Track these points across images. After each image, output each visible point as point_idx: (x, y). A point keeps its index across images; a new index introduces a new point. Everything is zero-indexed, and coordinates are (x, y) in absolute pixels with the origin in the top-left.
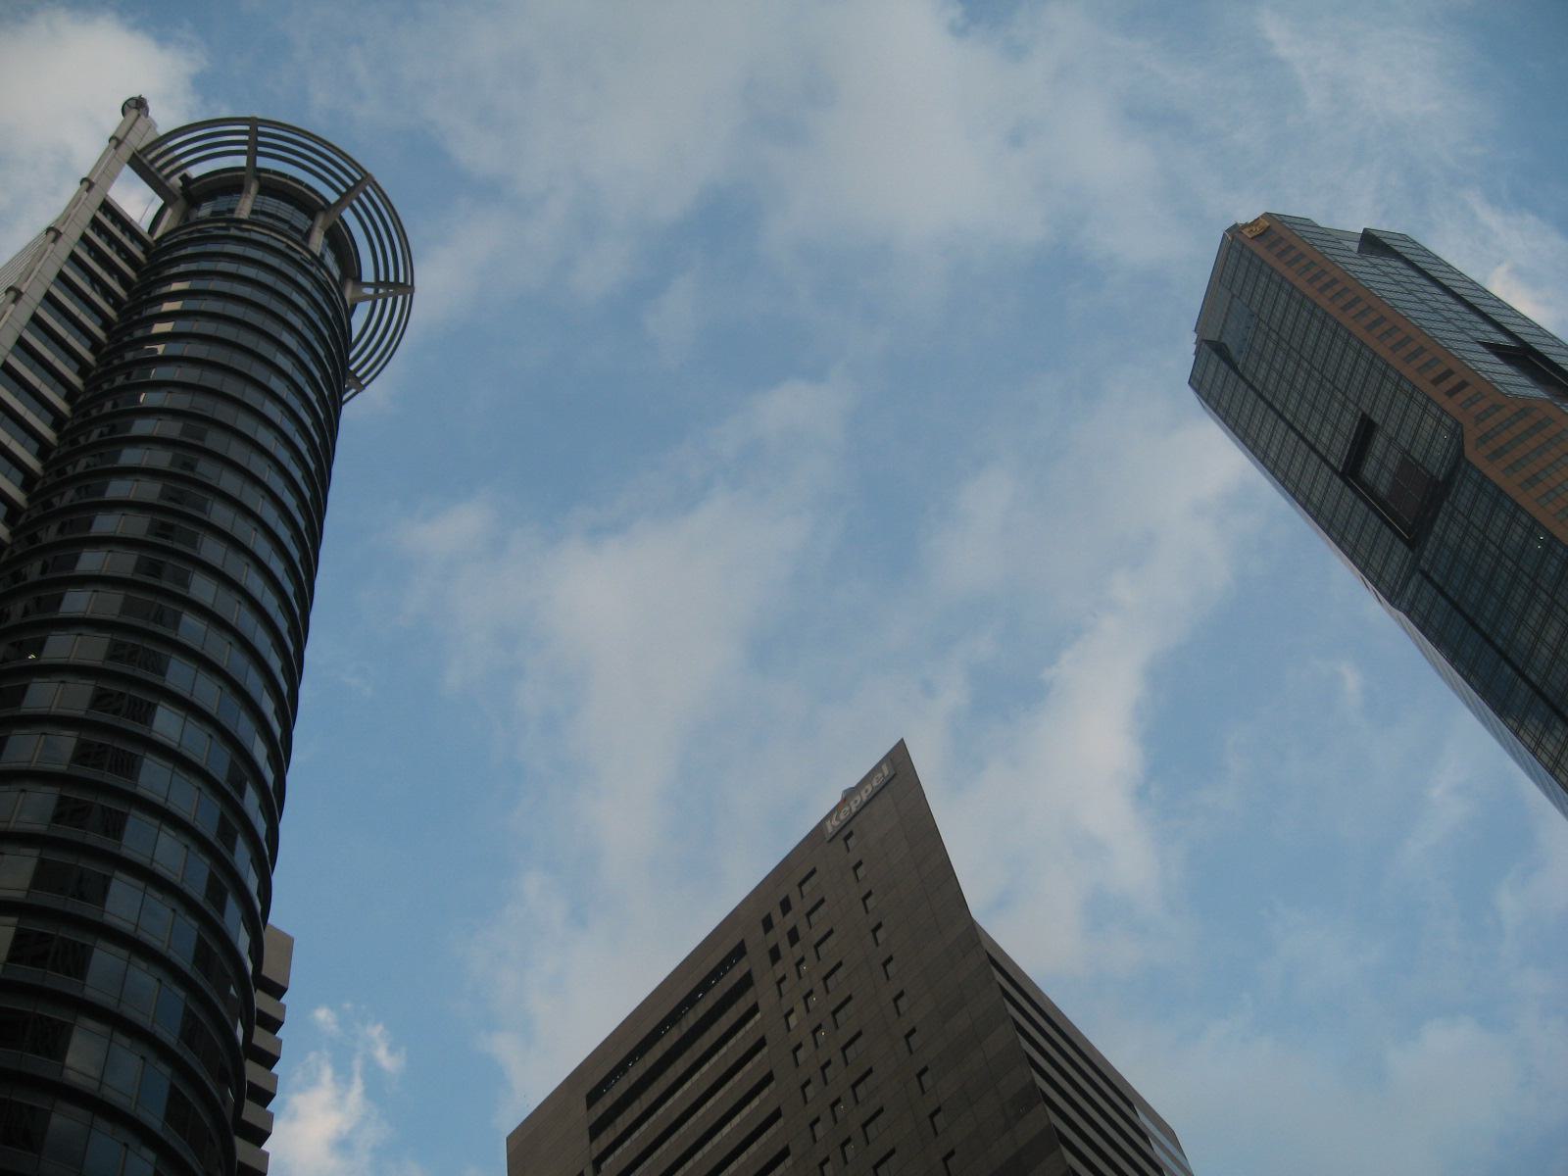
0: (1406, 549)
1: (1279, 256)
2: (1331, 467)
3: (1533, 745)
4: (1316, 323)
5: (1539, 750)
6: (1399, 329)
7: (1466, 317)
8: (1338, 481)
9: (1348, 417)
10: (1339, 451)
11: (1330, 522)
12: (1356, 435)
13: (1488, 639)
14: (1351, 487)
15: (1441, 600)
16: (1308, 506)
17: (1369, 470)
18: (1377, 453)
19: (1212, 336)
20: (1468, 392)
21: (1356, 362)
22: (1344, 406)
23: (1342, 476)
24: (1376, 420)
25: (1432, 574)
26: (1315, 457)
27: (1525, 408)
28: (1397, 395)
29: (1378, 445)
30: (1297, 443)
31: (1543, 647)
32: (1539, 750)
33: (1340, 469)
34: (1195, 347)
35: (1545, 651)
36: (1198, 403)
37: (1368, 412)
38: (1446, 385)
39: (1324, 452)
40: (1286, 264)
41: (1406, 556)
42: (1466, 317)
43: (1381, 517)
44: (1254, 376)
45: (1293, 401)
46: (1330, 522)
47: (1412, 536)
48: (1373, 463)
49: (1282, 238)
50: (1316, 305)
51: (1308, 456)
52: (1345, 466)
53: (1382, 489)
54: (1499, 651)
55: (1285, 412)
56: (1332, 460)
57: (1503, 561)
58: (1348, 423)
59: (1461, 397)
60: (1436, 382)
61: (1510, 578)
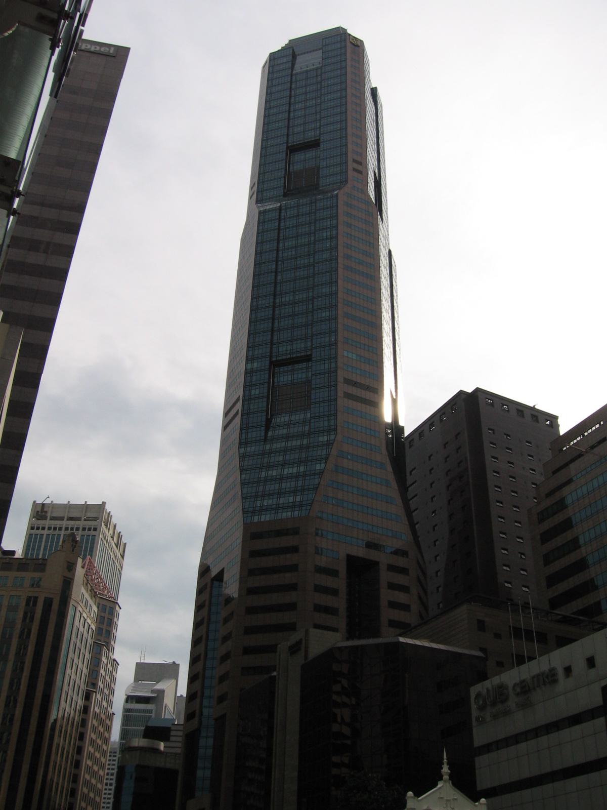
0: (282, 194)
2: (287, 141)
4: (339, 72)
8: (285, 147)
10: (296, 139)
11: (268, 124)
12: (308, 142)
13: (289, 112)
14: (287, 154)
16: (257, 266)
17: (299, 156)
18: (307, 156)
19: (297, 51)
21: (337, 114)
22: (315, 129)
23: (288, 147)
24: (322, 146)
25: (283, 211)
28: (338, 140)
29: (310, 154)
30: (288, 82)
31: (282, 456)
33: (290, 145)
34: (280, 48)
38: (356, 166)
39: (290, 133)
44: (295, 103)
45: (300, 106)
46: (268, 124)
47: (289, 193)
48: (302, 157)
50: (346, 89)
52: (292, 146)
55: (283, 221)
56: (290, 139)
58: (310, 136)
60: (354, 161)
61: (293, 414)
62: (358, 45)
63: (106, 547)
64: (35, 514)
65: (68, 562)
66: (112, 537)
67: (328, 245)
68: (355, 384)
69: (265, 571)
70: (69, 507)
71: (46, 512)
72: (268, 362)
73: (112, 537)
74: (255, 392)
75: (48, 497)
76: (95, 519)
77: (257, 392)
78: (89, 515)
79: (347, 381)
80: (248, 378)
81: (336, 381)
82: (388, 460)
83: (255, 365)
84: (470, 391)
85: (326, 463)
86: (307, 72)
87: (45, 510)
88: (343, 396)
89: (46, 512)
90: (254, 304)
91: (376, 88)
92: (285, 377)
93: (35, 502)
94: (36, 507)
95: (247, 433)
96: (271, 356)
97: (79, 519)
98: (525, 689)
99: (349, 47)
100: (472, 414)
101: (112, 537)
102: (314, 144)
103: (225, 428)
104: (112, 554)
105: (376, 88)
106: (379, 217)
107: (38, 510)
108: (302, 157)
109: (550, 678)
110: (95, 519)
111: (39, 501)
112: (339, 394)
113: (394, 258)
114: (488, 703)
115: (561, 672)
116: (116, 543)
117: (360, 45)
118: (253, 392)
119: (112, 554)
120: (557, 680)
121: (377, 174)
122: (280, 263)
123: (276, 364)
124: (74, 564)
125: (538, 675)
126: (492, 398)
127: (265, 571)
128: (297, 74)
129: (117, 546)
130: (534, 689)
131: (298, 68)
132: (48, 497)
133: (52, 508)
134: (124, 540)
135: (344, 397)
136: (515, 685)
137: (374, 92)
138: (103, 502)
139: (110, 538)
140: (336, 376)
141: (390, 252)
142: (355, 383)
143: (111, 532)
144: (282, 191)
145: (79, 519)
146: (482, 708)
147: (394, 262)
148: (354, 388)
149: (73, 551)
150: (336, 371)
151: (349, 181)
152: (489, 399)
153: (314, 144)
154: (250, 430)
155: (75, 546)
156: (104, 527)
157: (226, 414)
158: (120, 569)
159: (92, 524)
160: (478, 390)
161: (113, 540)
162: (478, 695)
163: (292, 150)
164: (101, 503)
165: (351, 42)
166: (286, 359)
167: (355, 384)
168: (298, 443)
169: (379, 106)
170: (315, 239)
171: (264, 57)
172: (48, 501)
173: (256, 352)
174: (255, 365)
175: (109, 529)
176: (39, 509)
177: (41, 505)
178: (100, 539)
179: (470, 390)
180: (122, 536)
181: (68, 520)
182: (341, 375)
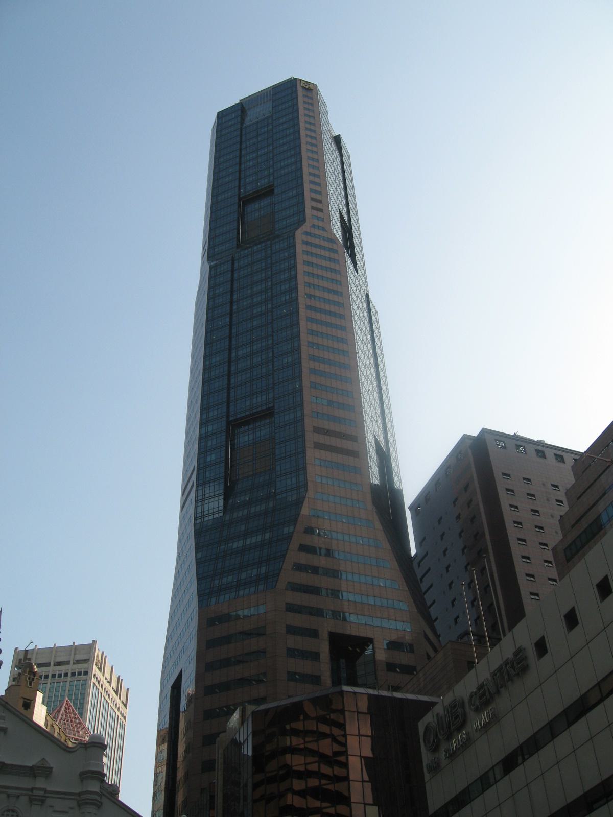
0: (236, 246)
1: (304, 96)
3: (200, 498)
5: (200, 504)
6: (319, 170)
7: (363, 301)
8: (237, 199)
9: (266, 180)
15: (237, 174)
17: (251, 207)
20: (320, 214)
24: (276, 191)
26: (229, 275)
27: (333, 240)
29: (264, 202)
32: (200, 504)
35: (249, 291)
36: (214, 121)
37: (275, 185)
40: (304, 107)
41: (218, 512)
42: (363, 301)
43: (227, 458)
49: (314, 117)
51: (226, 293)
53: (241, 440)
54: (229, 371)
57: (269, 338)
58: (263, 183)
59: (315, 213)
62: (310, 89)
63: (101, 694)
64: (18, 662)
65: (24, 698)
66: (108, 682)
67: (287, 287)
68: (327, 433)
69: (226, 663)
70: (56, 651)
71: (30, 659)
72: (224, 423)
73: (110, 682)
74: (212, 458)
75: (32, 642)
76: (86, 661)
77: (213, 457)
78: (78, 657)
79: (317, 430)
80: (203, 444)
81: (303, 430)
82: (376, 517)
83: (210, 428)
84: (476, 435)
85: (295, 525)
86: (257, 122)
87: (29, 656)
88: (313, 447)
89: (30, 659)
90: (207, 363)
91: (339, 136)
92: (245, 437)
93: (16, 649)
94: (18, 654)
95: (203, 505)
96: (228, 416)
97: (67, 663)
98: (484, 698)
99: (300, 92)
100: (483, 469)
101: (110, 682)
102: (269, 191)
103: (183, 507)
104: (110, 702)
105: (339, 136)
106: (350, 264)
107: (20, 658)
108: (257, 206)
109: (517, 666)
110: (86, 661)
111: (22, 648)
112: (307, 445)
113: (373, 302)
114: (441, 737)
115: (531, 652)
116: (116, 690)
117: (312, 88)
118: (209, 459)
119: (110, 702)
120: (528, 665)
121: (346, 217)
122: (234, 315)
123: (234, 425)
124: (31, 700)
125: (500, 669)
126: (503, 439)
127: (226, 663)
128: (247, 127)
129: (116, 693)
130: (498, 692)
131: (247, 122)
132: (32, 642)
133: (37, 653)
134: (125, 686)
135: (315, 448)
136: (471, 697)
137: (337, 140)
138: (93, 641)
139: (106, 685)
140: (303, 425)
141: (367, 295)
142: (327, 432)
143: (107, 675)
144: (235, 242)
145: (67, 663)
146: (435, 749)
147: (375, 308)
148: (326, 437)
149: (30, 684)
150: (303, 420)
151: (307, 220)
152: (500, 441)
153: (269, 191)
154: (206, 502)
155: (33, 679)
156: (97, 670)
157: (183, 492)
158: (123, 720)
159: (82, 667)
160: (484, 431)
161: (110, 685)
162: (427, 729)
163: (245, 201)
164: (91, 643)
165: (303, 87)
166: (246, 416)
167: (327, 433)
168: (263, 507)
169: (344, 153)
170: (272, 284)
171: (211, 120)
172: (31, 647)
173: (211, 414)
174: (210, 428)
175: (104, 672)
176: (22, 657)
177: (23, 653)
178: (92, 683)
179: (475, 433)
180: (122, 680)
181: (54, 666)
182: (309, 423)
